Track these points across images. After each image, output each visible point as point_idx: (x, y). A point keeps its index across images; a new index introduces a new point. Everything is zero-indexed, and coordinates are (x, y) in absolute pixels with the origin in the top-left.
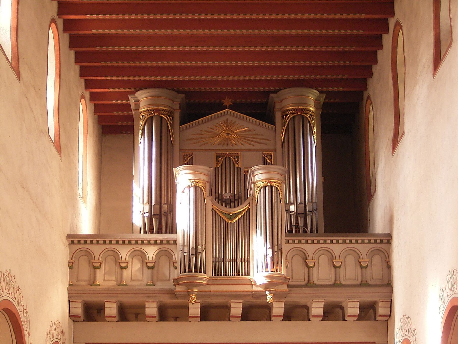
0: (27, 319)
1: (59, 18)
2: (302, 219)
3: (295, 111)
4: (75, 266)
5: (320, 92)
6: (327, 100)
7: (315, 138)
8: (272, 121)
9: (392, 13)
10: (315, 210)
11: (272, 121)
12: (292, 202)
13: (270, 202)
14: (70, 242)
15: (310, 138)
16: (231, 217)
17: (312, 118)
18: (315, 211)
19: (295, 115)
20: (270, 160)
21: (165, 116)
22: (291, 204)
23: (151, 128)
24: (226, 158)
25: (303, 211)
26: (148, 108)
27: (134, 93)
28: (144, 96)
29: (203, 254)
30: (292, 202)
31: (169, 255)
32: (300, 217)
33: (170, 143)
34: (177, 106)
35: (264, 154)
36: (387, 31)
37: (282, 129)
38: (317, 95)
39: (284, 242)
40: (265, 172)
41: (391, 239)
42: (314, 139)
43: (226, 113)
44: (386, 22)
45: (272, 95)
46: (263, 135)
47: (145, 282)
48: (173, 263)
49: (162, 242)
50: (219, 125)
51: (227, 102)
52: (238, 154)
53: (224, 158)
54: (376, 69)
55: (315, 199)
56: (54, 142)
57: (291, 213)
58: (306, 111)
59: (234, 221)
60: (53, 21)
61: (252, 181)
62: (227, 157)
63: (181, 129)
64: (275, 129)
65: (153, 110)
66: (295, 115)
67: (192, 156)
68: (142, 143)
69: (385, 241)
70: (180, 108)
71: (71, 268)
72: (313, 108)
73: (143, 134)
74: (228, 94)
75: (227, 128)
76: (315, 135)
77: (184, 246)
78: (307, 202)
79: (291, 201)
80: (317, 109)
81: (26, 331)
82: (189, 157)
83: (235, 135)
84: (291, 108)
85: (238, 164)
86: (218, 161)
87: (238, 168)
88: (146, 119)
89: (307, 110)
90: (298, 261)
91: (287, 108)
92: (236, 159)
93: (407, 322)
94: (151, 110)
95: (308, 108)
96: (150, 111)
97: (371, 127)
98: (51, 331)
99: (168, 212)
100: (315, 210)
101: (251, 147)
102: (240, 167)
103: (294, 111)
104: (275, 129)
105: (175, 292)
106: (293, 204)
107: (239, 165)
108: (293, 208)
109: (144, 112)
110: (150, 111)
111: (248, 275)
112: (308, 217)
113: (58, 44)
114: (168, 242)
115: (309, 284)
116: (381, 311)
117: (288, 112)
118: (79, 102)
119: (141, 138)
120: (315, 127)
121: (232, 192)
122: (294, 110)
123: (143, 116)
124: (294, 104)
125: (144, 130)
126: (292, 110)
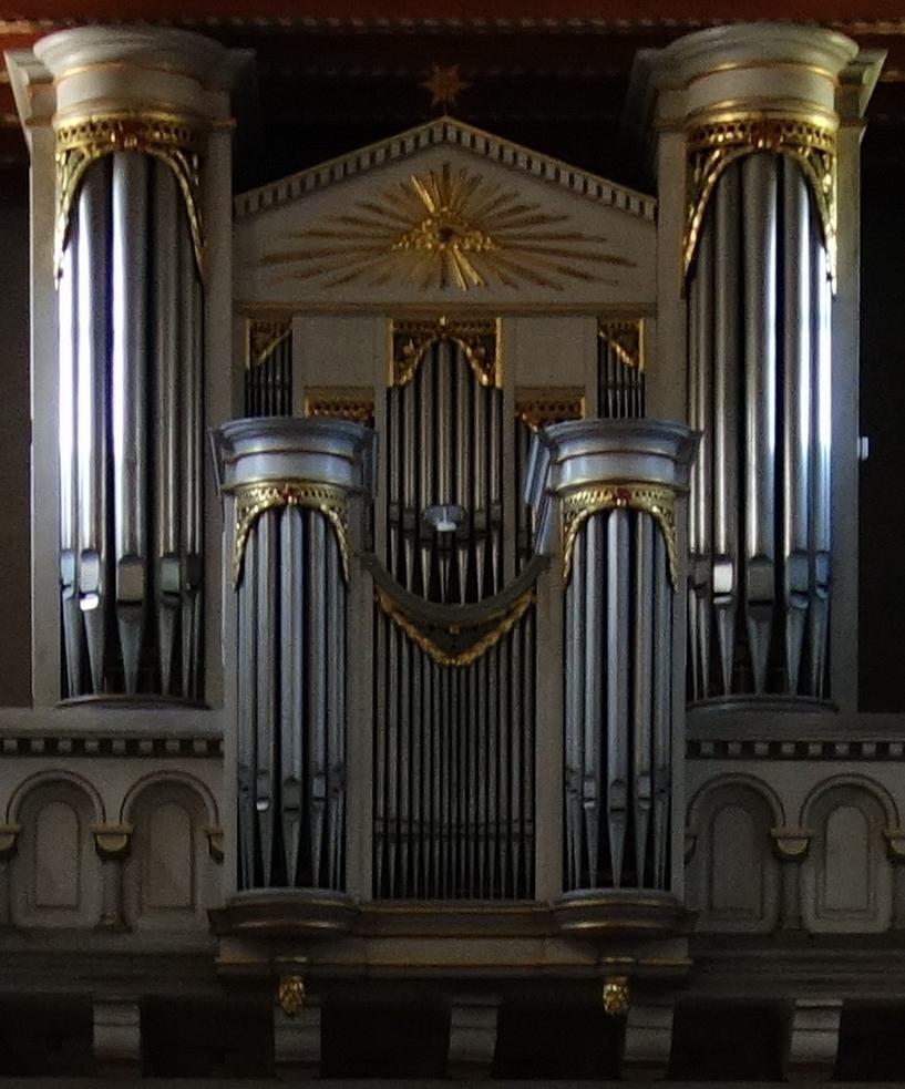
2: (766, 627)
5: (866, 42)
6: (893, 74)
10: (821, 586)
11: (642, 178)
12: (722, 550)
13: (626, 550)
15: (791, 444)
18: (821, 593)
19: (749, 149)
20: (630, 354)
21: (169, 154)
22: (715, 558)
24: (435, 347)
25: (770, 593)
27: (26, 43)
28: (73, 58)
30: (722, 550)
31: (189, 798)
32: (754, 617)
34: (222, 101)
37: (688, 216)
38: (846, 58)
39: (680, 749)
40: (601, 449)
42: (829, 261)
45: (645, 54)
47: (91, 917)
49: (159, 747)
51: (443, 83)
53: (428, 343)
55: (824, 538)
57: (718, 600)
59: (467, 658)
61: (549, 484)
62: (440, 340)
63: (241, 211)
64: (656, 210)
65: (116, 127)
72: (827, 116)
76: (832, 243)
77: (257, 773)
78: (787, 553)
82: (274, 336)
86: (400, 357)
88: (81, 166)
89: (800, 130)
91: (713, 120)
92: (482, 351)
100: (821, 586)
101: (545, 295)
102: (498, 384)
104: (656, 210)
106: (723, 559)
107: (492, 377)
108: (724, 577)
111: (522, 896)
112: (789, 617)
114: (186, 747)
115: (788, 933)
117: (716, 140)
119: (64, 248)
120: (833, 207)
121: (460, 502)
123: (68, 152)
125: (73, 215)
126: (731, 129)
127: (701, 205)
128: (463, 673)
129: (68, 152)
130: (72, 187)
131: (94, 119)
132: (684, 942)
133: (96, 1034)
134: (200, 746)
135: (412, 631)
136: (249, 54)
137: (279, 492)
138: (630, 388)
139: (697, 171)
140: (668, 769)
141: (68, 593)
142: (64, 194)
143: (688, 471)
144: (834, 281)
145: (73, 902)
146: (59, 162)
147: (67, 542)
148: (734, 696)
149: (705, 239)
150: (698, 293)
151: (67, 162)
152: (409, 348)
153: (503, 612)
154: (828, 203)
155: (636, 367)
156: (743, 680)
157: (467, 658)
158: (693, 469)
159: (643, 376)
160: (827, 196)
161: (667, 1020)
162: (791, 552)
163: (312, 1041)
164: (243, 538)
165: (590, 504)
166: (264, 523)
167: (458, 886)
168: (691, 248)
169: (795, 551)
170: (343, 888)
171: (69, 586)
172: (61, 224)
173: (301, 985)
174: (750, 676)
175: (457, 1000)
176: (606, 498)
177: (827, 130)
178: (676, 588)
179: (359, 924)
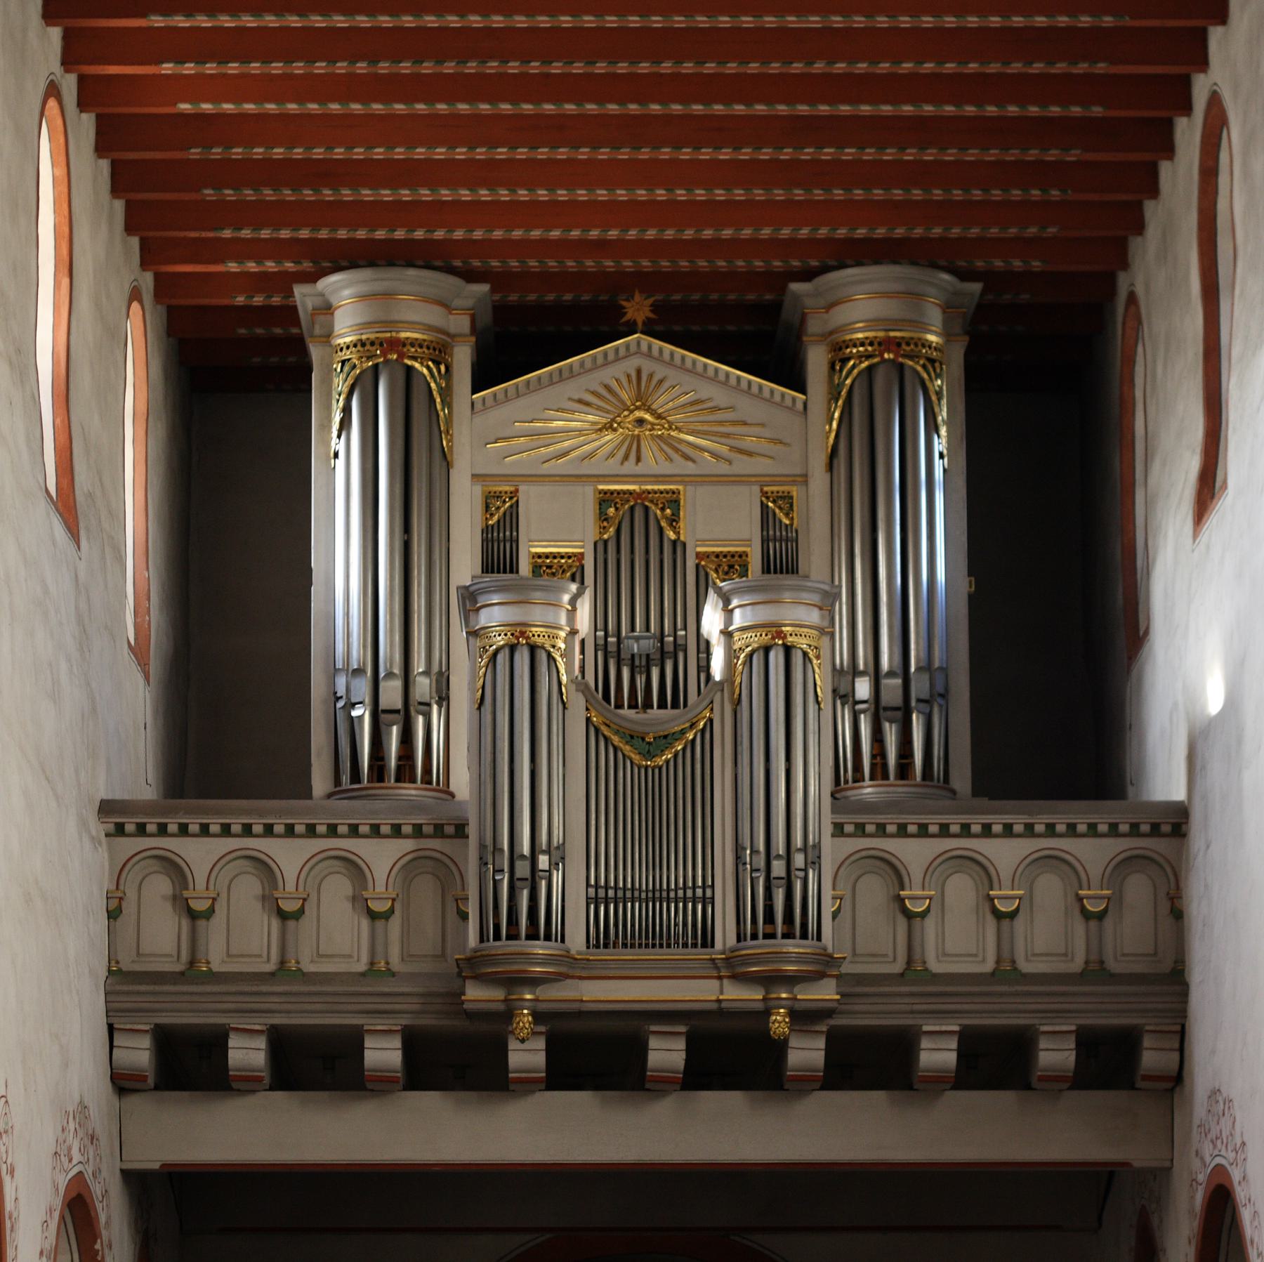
0: (7, 1124)
1: (67, 71)
3: (876, 346)
4: (129, 908)
7: (944, 441)
8: (797, 382)
9: (1202, 63)
11: (797, 382)
12: (861, 667)
14: (111, 827)
16: (652, 750)
17: (935, 370)
18: (939, 700)
19: (876, 360)
20: (787, 515)
21: (422, 364)
22: (855, 672)
23: (371, 404)
24: (632, 509)
26: (362, 334)
29: (557, 878)
33: (437, 454)
34: (460, 323)
35: (764, 494)
36: (1186, 107)
37: (830, 409)
39: (828, 829)
41: (1187, 823)
42: (939, 445)
43: (633, 348)
44: (1185, 85)
45: (795, 287)
46: (763, 425)
48: (457, 900)
50: (608, 388)
51: (638, 308)
52: (674, 493)
53: (627, 507)
54: (1153, 212)
56: (54, 494)
57: (859, 707)
58: (912, 346)
59: (660, 761)
60: (53, 90)
63: (478, 406)
66: (876, 360)
67: (515, 499)
68: (342, 455)
69: (1166, 828)
70: (474, 330)
71: (113, 915)
73: (345, 424)
74: (644, 281)
75: (637, 401)
78: (913, 669)
79: (858, 664)
80: (947, 334)
81: (5, 1162)
82: (504, 502)
83: (666, 426)
84: (860, 335)
85: (675, 528)
86: (603, 517)
87: (674, 543)
90: (874, 891)
91: (848, 337)
93: (1224, 1114)
94: (372, 344)
95: (921, 335)
96: (368, 347)
97: (1138, 394)
98: (64, 1142)
99: (431, 698)
102: (682, 538)
103: (870, 348)
105: (463, 1002)
107: (678, 534)
108: (863, 689)
109: (348, 347)
110: (368, 347)
113: (63, 158)
115: (913, 971)
116: (1152, 1058)
117: (851, 352)
118: (125, 316)
119: (339, 437)
120: (944, 401)
122: (871, 344)
123: (343, 362)
124: (872, 323)
125: (347, 410)
126: (862, 345)
127: (840, 402)
128: (657, 771)
129: (343, 362)
130: (346, 390)
131: (364, 337)
132: (833, 982)
133: (365, 1055)
134: (450, 830)
135: (616, 739)
136: (484, 288)
137: (512, 635)
138: (787, 541)
139: (836, 378)
140: (817, 846)
141: (340, 704)
142: (340, 395)
143: (833, 605)
144: (946, 459)
145: (975, 952)
146: (336, 370)
147: (339, 665)
148: (872, 783)
149: (844, 426)
150: (839, 465)
151: (342, 370)
152: (611, 511)
153: (687, 725)
154: (939, 399)
155: (792, 525)
156: (879, 771)
157: (660, 761)
158: (837, 604)
159: (797, 531)
160: (939, 394)
161: (821, 1043)
162: (915, 670)
163: (539, 1059)
164: (484, 669)
165: (754, 642)
166: (502, 659)
167: (654, 938)
168: (833, 435)
169: (918, 669)
170: (563, 941)
171: (341, 697)
172: (337, 418)
173: (530, 1019)
174: (885, 765)
175: (653, 1028)
176: (766, 638)
177: (937, 343)
178: (822, 706)
179: (570, 968)
